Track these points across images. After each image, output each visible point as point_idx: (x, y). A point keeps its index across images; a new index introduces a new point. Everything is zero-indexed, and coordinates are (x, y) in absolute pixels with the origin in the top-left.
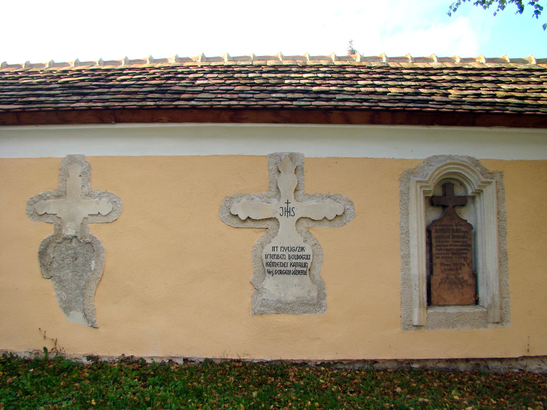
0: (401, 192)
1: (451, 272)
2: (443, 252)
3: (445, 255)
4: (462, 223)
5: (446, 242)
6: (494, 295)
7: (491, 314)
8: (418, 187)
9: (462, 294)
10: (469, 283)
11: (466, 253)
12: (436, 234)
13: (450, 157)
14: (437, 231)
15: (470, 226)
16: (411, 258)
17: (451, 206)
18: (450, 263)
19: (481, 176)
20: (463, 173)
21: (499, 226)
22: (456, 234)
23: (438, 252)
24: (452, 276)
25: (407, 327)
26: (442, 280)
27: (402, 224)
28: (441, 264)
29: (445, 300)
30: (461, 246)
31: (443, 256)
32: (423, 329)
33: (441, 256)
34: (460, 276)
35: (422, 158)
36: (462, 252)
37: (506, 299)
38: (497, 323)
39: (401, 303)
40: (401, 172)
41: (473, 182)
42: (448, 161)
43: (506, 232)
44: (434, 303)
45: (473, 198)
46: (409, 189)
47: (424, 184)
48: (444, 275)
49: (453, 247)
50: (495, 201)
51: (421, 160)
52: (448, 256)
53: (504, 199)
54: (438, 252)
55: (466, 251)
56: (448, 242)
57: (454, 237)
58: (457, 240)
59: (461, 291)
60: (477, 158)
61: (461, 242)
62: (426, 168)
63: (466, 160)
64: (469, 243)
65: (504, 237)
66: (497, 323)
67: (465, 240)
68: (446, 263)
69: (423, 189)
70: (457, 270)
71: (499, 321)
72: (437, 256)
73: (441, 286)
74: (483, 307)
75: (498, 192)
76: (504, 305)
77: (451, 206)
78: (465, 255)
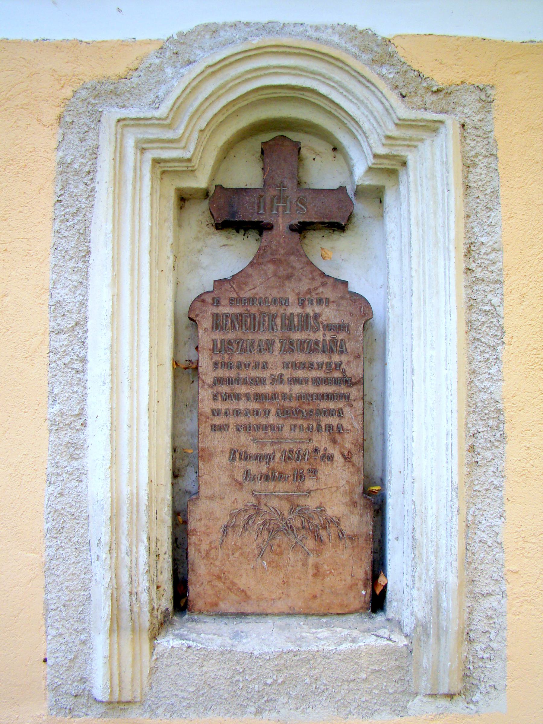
0: (64, 166)
1: (271, 485)
2: (242, 405)
3: (252, 420)
4: (328, 292)
5: (256, 366)
6: (438, 587)
7: (425, 662)
8: (130, 143)
9: (318, 572)
10: (347, 531)
11: (339, 413)
12: (218, 336)
13: (268, 28)
14: (218, 323)
15: (361, 306)
16: (89, 430)
17: (282, 224)
18: (268, 450)
19: (394, 99)
20: (323, 90)
21: (471, 304)
22: (297, 336)
23: (220, 405)
24: (275, 503)
25: (68, 702)
26: (233, 516)
27: (62, 293)
28: (233, 452)
29: (245, 596)
30: (317, 381)
31: (242, 420)
32: (134, 714)
33: (231, 421)
34: (311, 503)
35: (154, 36)
36: (324, 405)
37: (493, 602)
38: (451, 696)
39: (47, 610)
40: (68, 92)
41: (366, 126)
42: (256, 42)
43: (501, 328)
44: (200, 604)
45: (376, 195)
46: (95, 152)
47: (154, 133)
48: (244, 498)
49: (286, 388)
50: (454, 199)
51: (150, 42)
52: (263, 421)
53: (495, 193)
54: (220, 405)
55: (340, 405)
56: (265, 366)
57: (289, 346)
58: (301, 357)
59: (312, 559)
60: (384, 31)
61: (320, 366)
62: (169, 71)
63: (336, 39)
64: (353, 370)
65: (494, 348)
66: (451, 696)
67: (336, 358)
68: (253, 450)
69: (149, 156)
70: (299, 476)
71: (458, 686)
72: (217, 421)
73: (231, 540)
74: (399, 625)
75: (468, 166)
76: (480, 623)
77: (282, 224)
78: (334, 421)
